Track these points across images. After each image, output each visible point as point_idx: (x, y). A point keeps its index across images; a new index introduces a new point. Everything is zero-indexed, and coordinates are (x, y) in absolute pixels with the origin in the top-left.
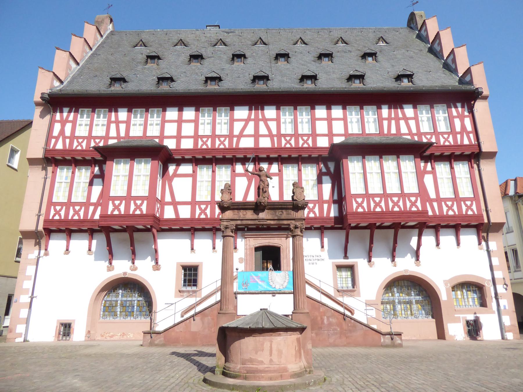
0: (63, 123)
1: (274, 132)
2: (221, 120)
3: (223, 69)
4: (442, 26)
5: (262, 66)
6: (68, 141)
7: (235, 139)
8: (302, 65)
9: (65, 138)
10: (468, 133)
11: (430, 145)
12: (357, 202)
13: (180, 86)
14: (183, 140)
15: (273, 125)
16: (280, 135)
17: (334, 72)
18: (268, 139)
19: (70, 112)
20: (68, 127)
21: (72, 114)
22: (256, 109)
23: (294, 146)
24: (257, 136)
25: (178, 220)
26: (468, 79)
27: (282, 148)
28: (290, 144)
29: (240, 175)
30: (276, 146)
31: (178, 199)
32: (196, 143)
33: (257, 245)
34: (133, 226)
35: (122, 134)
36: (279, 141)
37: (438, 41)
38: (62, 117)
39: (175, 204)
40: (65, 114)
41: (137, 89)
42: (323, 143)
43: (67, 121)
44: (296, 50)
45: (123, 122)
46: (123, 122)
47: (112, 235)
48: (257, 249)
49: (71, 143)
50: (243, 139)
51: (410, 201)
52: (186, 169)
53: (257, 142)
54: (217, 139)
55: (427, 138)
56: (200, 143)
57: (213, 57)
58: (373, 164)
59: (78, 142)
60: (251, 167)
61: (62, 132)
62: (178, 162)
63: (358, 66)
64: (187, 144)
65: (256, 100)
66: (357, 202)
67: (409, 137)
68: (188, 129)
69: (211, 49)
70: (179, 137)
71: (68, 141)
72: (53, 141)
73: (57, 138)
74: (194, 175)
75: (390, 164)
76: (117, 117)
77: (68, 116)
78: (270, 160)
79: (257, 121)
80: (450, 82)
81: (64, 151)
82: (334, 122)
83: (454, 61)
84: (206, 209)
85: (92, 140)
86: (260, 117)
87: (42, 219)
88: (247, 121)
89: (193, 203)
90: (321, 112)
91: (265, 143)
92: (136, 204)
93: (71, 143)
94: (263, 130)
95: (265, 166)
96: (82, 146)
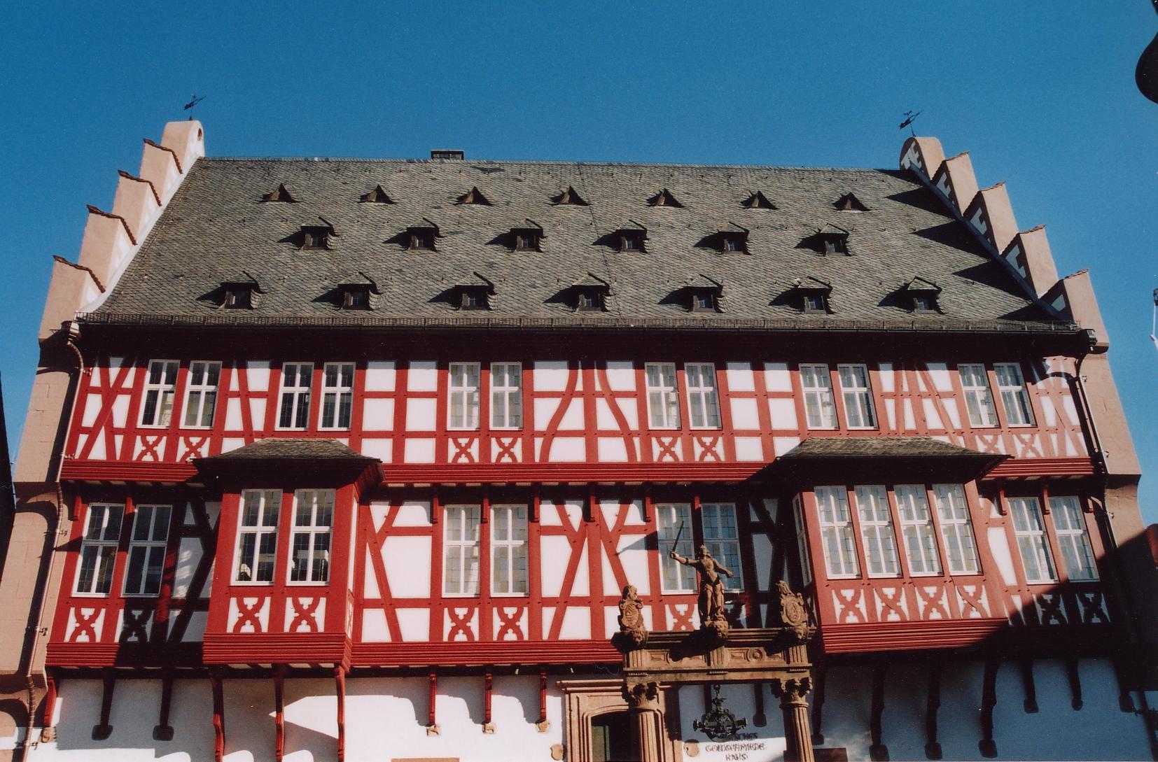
0: (109, 395)
1: (633, 424)
2: (165, 392)
3: (491, 265)
4: (987, 176)
5: (585, 258)
6: (119, 440)
7: (538, 442)
8: (680, 258)
9: (112, 432)
10: (112, 432)
11: (998, 459)
12: (842, 600)
13: (270, 308)
14: (410, 443)
15: (629, 407)
16: (646, 434)
17: (757, 280)
18: (619, 443)
19: (125, 366)
20: (121, 406)
21: (132, 371)
22: (588, 366)
23: (681, 459)
24: (591, 433)
25: (397, 644)
26: (1059, 304)
27: (653, 465)
28: (673, 454)
29: (551, 531)
30: (639, 459)
31: (397, 592)
32: (441, 450)
33: (598, 712)
34: (225, 666)
35: (258, 424)
36: (647, 449)
37: (979, 212)
38: (105, 377)
39: (390, 604)
40: (114, 372)
41: (288, 312)
42: (749, 451)
43: (118, 389)
44: (660, 220)
45: (259, 395)
46: (259, 395)
47: (229, 687)
48: (598, 721)
49: (128, 447)
50: (558, 443)
51: (925, 596)
52: (414, 514)
53: (591, 449)
54: (450, 441)
55: (985, 442)
56: (452, 450)
57: (461, 232)
58: (869, 508)
59: (145, 442)
60: (574, 511)
61: (105, 416)
62: (396, 499)
63: (699, 268)
64: (420, 452)
65: (588, 349)
66: (842, 600)
67: (945, 439)
68: (421, 415)
69: (454, 212)
70: (399, 434)
71: (119, 440)
72: (83, 439)
73: (93, 433)
74: (434, 530)
75: (908, 507)
76: (243, 381)
77: (121, 377)
78: (624, 495)
79: (590, 399)
80: (983, 307)
81: (110, 463)
82: (411, 403)
83: (1022, 259)
84: (468, 617)
85: (139, 438)
86: (598, 388)
87: (41, 643)
88: (566, 397)
89: (436, 604)
90: (739, 377)
91: (612, 451)
92: (298, 607)
93: (128, 447)
94: (606, 420)
95: (609, 510)
96: (154, 454)
